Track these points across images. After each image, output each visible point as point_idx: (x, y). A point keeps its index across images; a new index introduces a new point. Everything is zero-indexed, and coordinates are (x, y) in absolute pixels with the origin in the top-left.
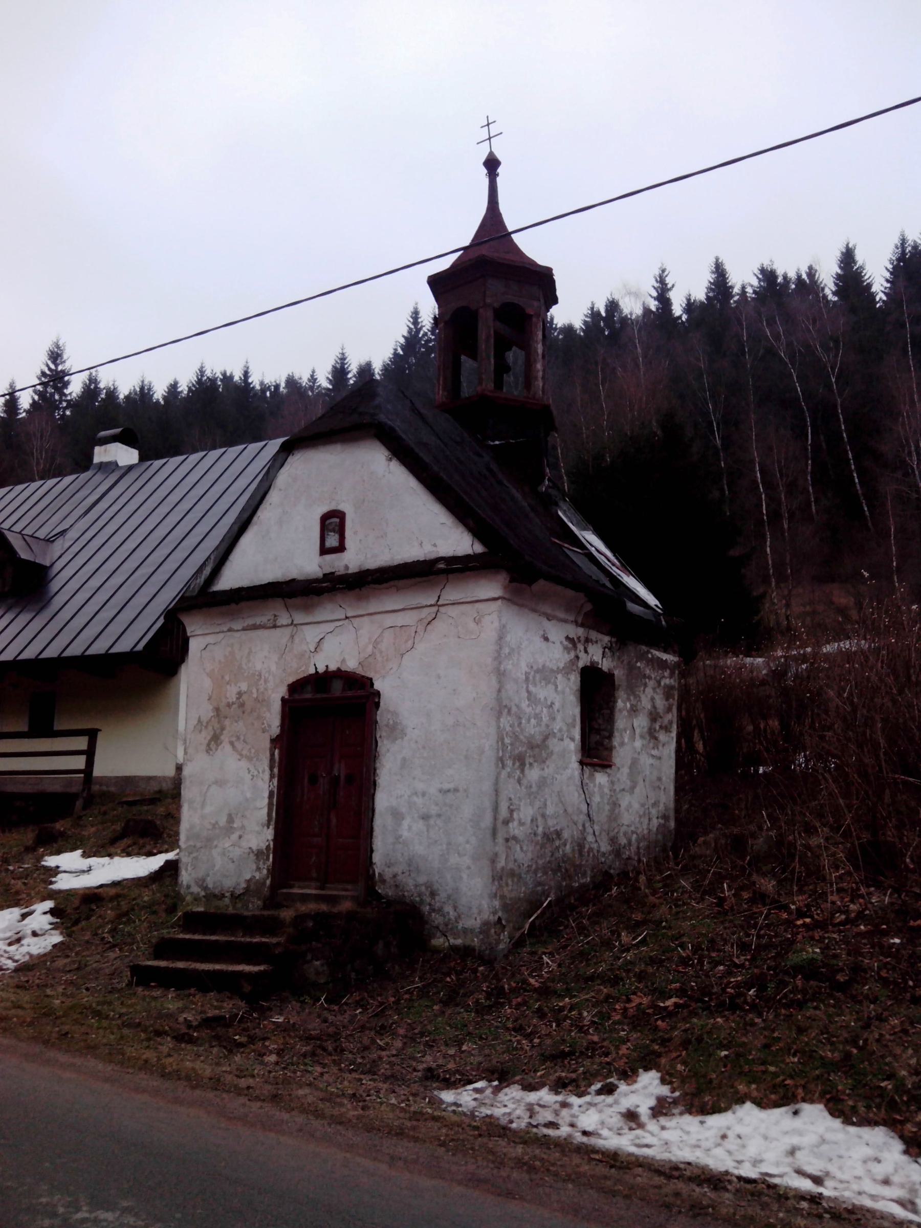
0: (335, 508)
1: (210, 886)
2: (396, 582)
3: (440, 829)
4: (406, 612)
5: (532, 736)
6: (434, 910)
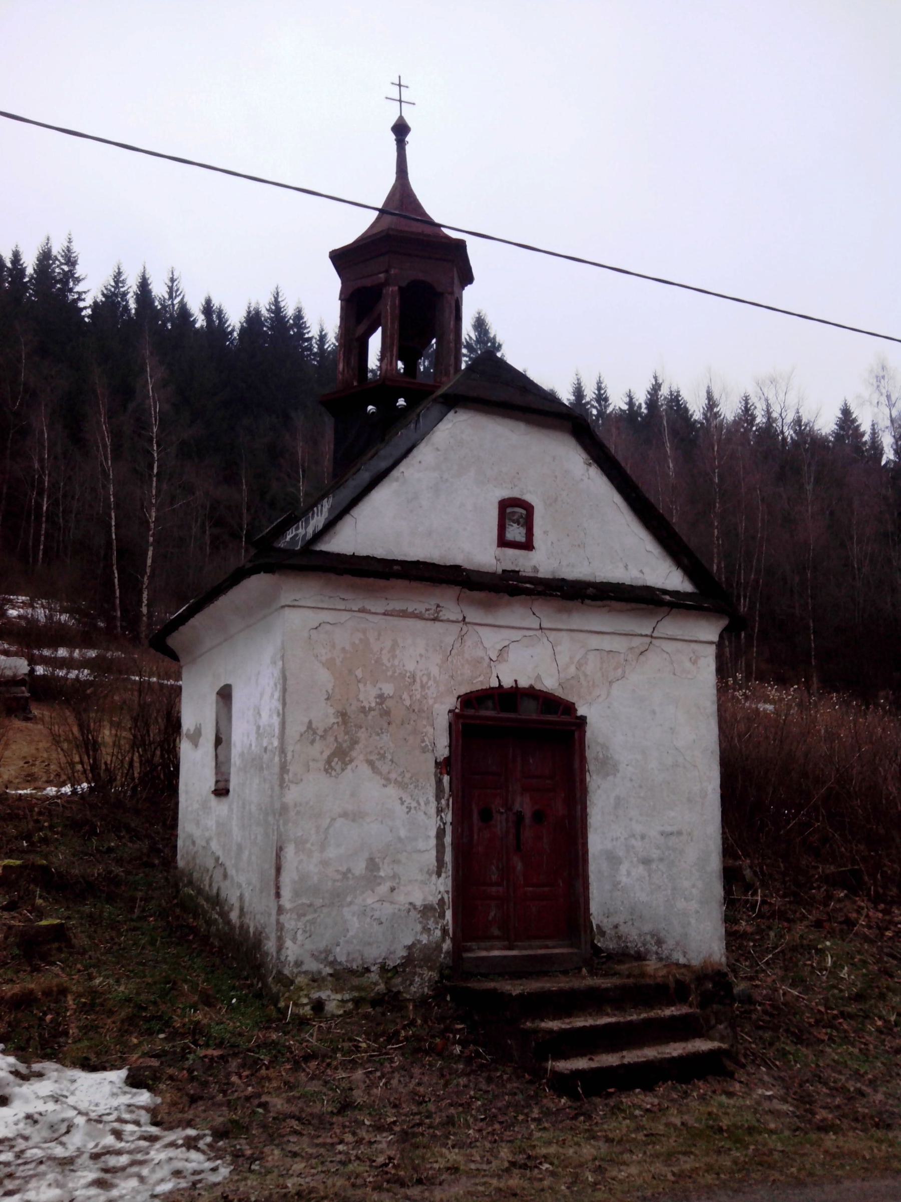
0: (518, 496)
3: (663, 873)
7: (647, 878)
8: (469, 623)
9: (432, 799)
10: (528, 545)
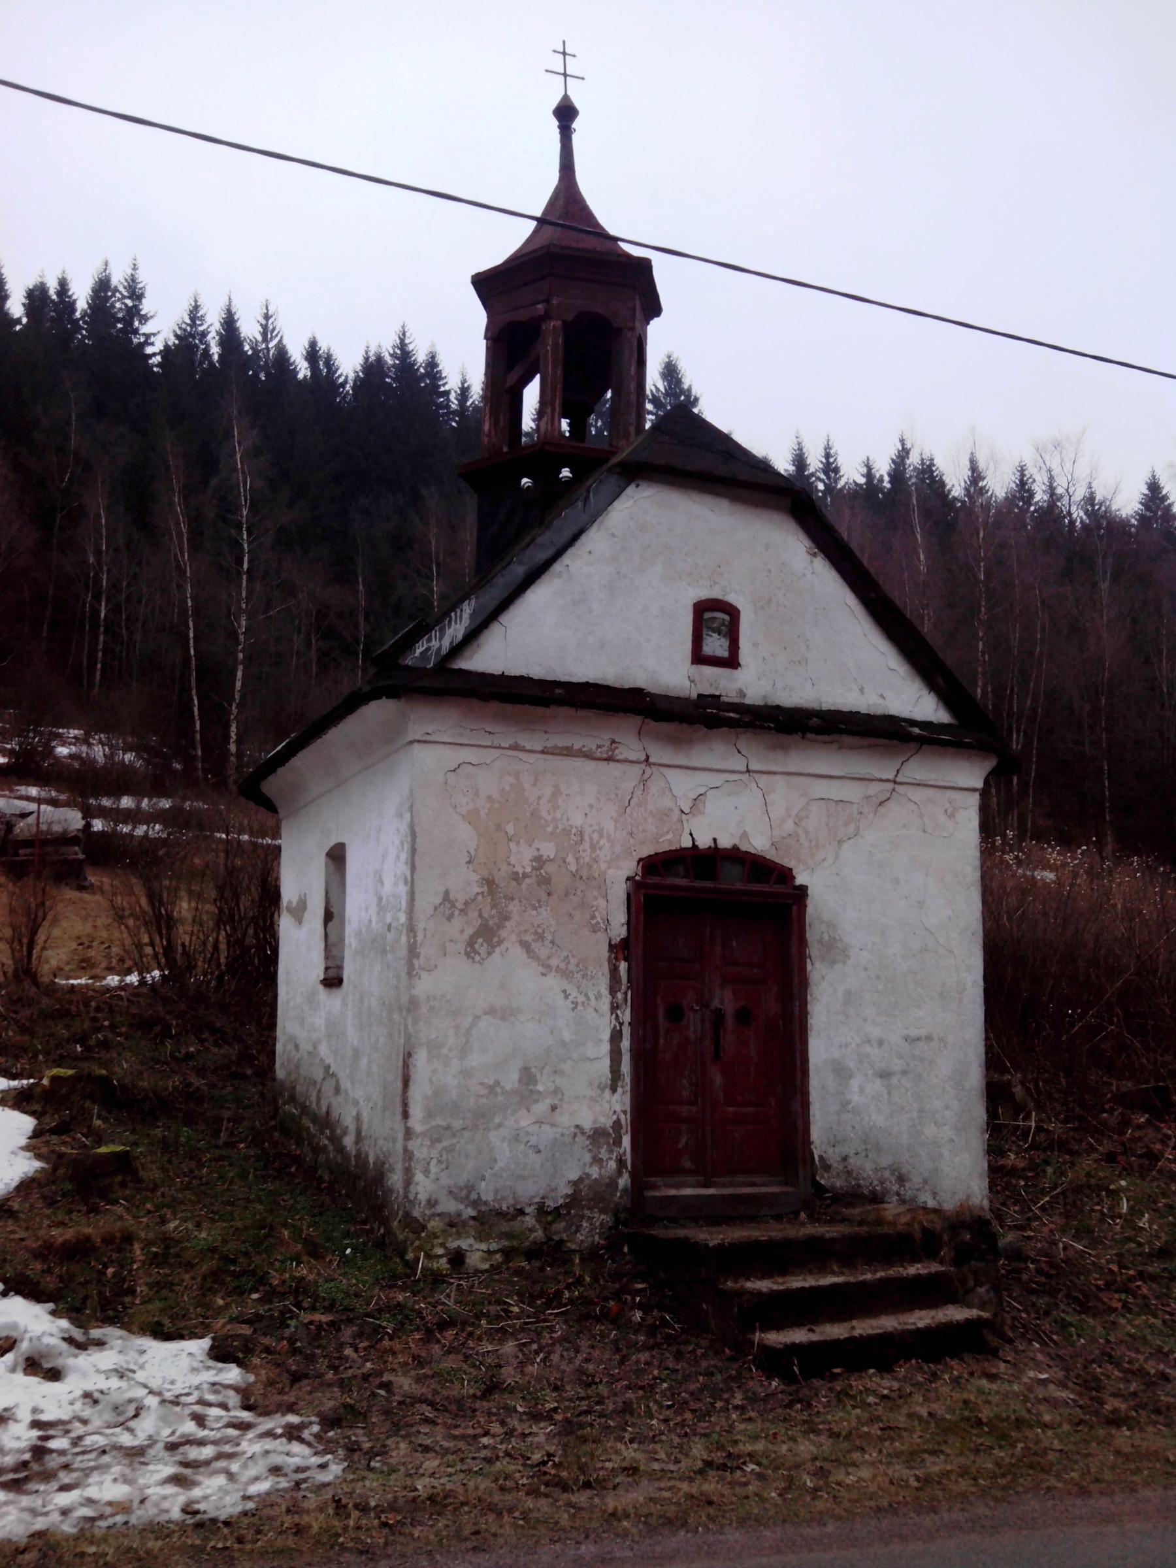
0: (721, 597)
3: (907, 1090)
7: (886, 1097)
8: (654, 764)
10: (731, 662)
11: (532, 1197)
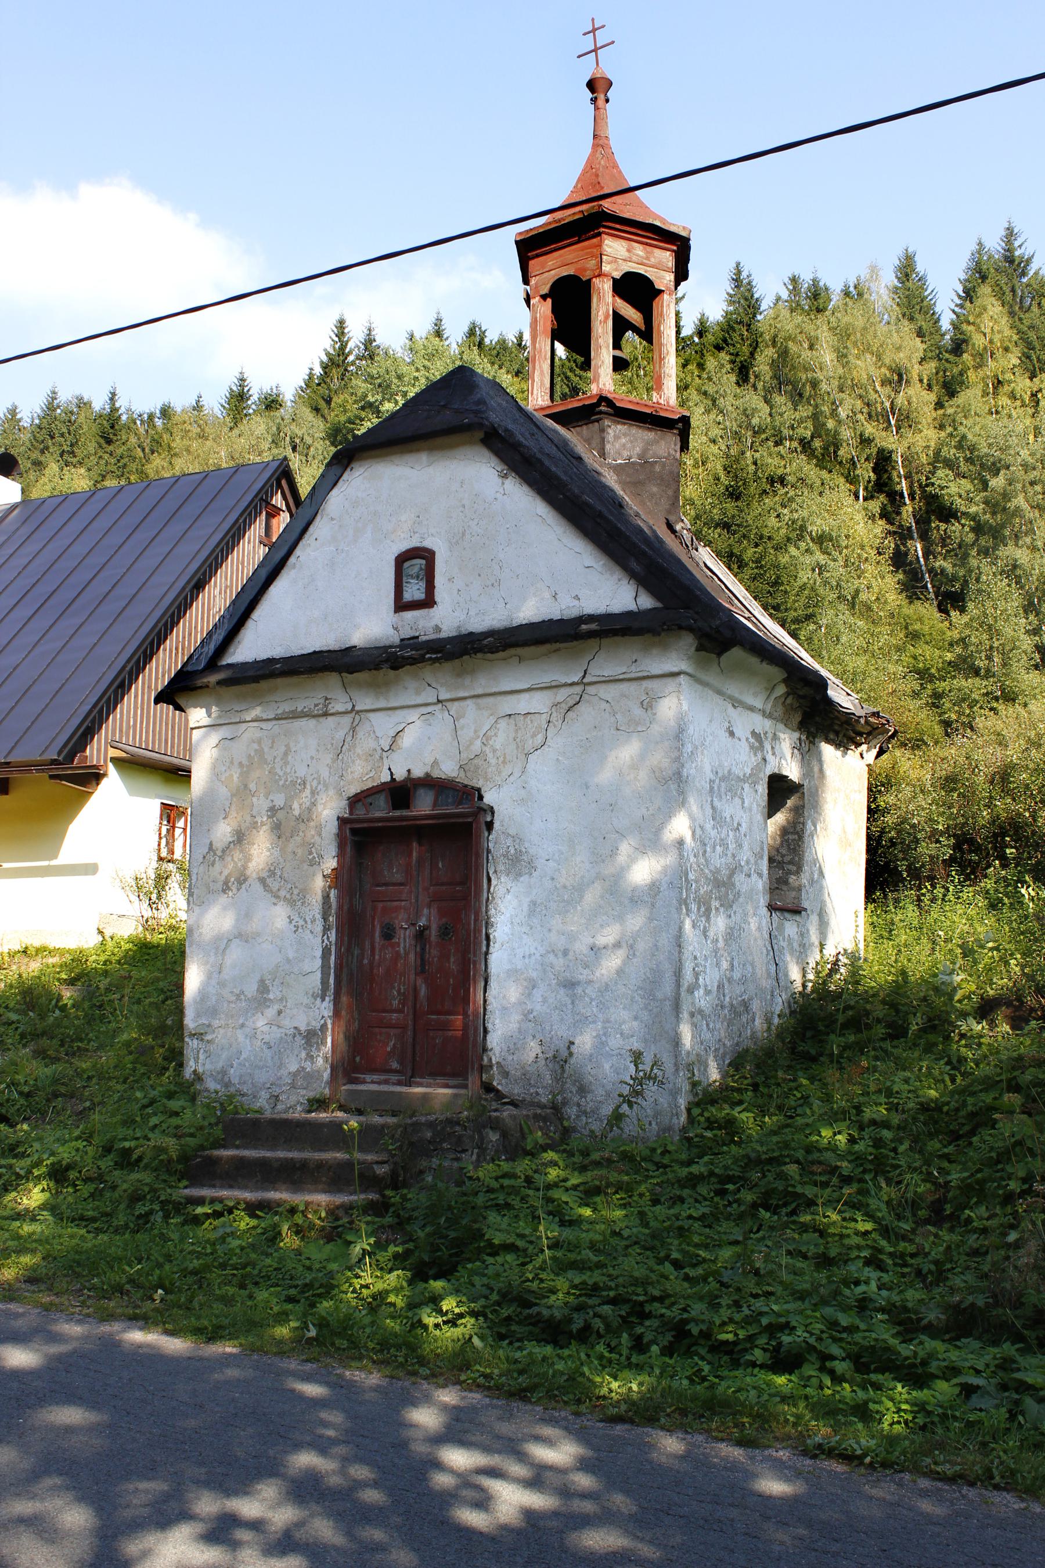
0: (418, 545)
1: (235, 1081)
2: (519, 651)
3: (592, 1000)
4: (532, 693)
5: (718, 871)
6: (585, 1113)
7: (570, 1006)
8: (361, 711)
9: (318, 917)
10: (428, 602)
11: (265, 1083)
